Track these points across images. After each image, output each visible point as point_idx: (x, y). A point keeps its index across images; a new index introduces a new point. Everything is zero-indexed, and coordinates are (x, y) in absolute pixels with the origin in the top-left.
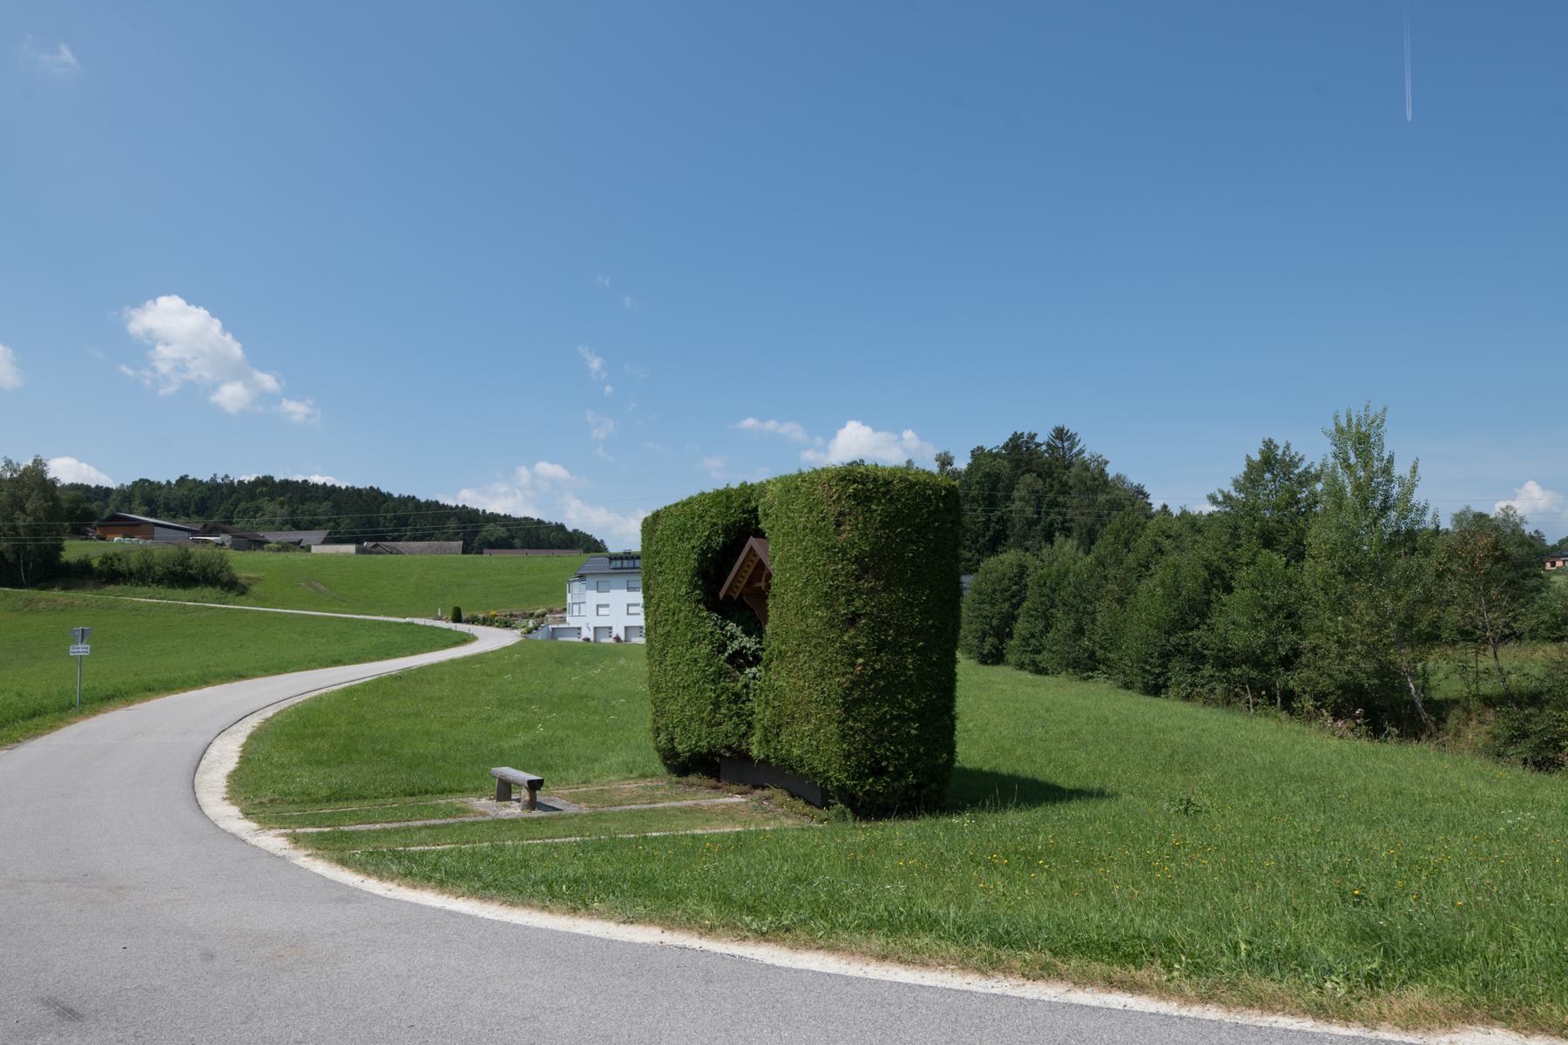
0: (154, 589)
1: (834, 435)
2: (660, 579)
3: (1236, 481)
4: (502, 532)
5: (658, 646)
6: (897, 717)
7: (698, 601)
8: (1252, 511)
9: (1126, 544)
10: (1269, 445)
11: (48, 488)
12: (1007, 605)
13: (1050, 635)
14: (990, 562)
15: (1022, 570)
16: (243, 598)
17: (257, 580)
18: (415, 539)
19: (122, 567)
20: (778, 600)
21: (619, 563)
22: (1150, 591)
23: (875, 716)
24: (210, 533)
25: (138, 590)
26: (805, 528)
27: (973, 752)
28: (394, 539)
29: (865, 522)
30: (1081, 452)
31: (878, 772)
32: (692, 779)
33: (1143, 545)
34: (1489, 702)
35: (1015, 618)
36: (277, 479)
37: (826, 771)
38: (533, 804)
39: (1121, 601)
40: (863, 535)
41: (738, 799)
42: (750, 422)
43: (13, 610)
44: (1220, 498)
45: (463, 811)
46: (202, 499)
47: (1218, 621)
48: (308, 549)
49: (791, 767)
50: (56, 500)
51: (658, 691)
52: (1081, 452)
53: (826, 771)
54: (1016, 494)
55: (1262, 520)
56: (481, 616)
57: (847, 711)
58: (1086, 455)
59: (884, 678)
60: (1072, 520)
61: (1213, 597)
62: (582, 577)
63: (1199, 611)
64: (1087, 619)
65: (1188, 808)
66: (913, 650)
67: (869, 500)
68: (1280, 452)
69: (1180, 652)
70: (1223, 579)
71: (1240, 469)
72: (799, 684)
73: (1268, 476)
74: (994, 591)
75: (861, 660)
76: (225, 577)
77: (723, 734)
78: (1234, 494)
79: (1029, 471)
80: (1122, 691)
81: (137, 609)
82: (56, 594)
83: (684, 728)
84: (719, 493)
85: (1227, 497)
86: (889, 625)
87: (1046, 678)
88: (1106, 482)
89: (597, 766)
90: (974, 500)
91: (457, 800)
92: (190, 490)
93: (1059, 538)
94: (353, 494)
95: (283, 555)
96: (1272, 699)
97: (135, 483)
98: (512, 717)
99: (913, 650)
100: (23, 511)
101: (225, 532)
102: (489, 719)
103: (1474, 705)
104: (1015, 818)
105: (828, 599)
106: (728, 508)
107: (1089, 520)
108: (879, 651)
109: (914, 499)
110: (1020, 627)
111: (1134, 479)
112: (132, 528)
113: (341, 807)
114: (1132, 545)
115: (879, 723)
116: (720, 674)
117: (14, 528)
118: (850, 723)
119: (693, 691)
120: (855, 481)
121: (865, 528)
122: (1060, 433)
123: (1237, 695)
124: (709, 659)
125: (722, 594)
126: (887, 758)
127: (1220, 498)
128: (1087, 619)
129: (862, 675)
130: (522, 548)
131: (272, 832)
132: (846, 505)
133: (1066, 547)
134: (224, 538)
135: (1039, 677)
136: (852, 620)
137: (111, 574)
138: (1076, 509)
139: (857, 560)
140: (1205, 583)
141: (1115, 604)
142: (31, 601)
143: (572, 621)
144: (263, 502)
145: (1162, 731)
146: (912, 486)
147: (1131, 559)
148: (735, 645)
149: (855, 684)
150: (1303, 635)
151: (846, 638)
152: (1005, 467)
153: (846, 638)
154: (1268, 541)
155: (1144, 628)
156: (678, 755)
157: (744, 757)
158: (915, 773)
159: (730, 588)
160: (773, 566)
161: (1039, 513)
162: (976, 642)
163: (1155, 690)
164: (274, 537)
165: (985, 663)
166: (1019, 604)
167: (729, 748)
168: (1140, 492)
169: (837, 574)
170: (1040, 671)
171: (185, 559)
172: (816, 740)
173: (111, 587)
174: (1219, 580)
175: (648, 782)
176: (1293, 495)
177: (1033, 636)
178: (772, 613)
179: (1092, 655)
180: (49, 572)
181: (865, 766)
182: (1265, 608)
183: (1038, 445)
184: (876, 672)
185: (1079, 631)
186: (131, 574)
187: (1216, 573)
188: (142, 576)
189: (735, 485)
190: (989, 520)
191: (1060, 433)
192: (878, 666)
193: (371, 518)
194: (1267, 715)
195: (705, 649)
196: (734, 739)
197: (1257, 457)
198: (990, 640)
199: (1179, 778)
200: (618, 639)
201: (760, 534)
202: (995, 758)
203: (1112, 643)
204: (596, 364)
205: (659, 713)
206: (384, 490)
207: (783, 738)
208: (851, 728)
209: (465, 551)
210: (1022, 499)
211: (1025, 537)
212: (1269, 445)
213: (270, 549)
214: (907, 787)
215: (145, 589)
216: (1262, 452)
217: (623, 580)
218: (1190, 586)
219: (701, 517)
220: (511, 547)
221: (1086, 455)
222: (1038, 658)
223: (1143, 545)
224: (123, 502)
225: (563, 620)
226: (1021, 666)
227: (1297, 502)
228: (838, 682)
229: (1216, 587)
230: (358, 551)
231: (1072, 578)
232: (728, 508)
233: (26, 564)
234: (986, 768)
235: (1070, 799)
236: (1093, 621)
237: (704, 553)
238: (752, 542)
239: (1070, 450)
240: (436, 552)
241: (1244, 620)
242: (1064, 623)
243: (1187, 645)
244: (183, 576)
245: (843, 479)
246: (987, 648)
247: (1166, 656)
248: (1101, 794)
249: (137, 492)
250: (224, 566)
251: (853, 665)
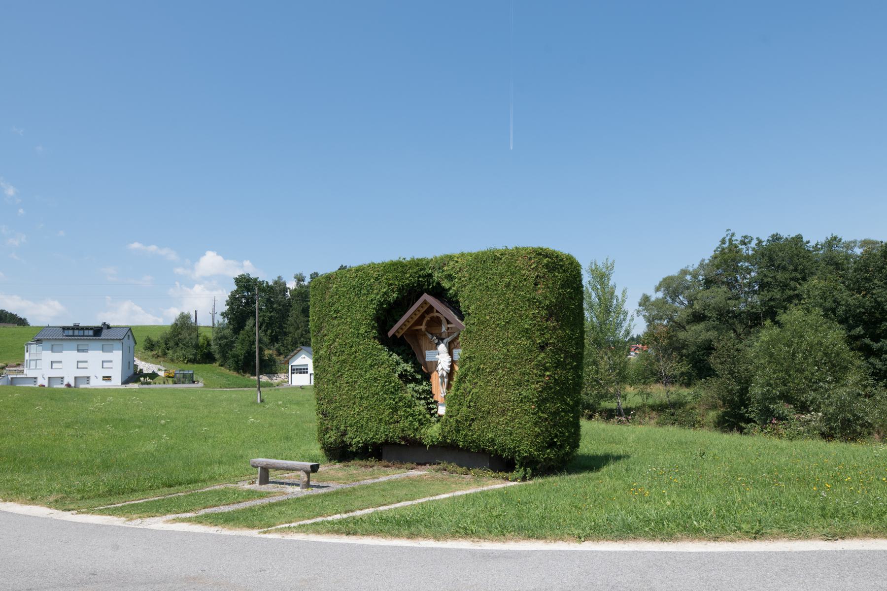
1: (198, 260)
7: (374, 338)
21: (71, 332)
31: (551, 445)
34: (653, 408)
42: (136, 245)
57: (539, 407)
62: (39, 341)
75: (548, 373)
103: (647, 410)
108: (557, 367)
115: (556, 413)
125: (390, 334)
131: (165, 518)
136: (542, 348)
139: (548, 308)
143: (28, 373)
149: (544, 389)
167: (404, 438)
169: (535, 317)
200: (69, 385)
204: (11, 191)
217: (74, 344)
225: (22, 372)
237: (381, 304)
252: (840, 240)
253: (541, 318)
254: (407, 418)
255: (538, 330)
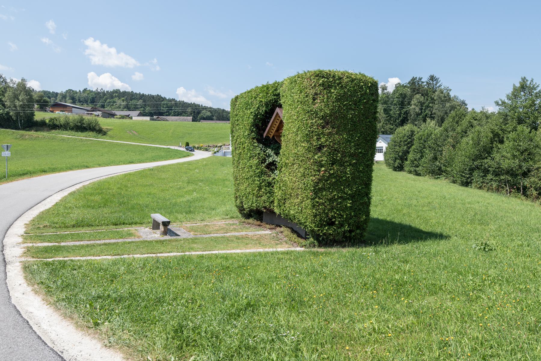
0: (70, 132)
2: (237, 128)
3: (508, 96)
4: (209, 114)
5: (236, 159)
6: (341, 197)
7: (254, 138)
8: (514, 108)
9: (457, 123)
10: (524, 80)
11: (29, 92)
12: (405, 147)
13: (423, 160)
14: (400, 129)
15: (413, 132)
16: (104, 136)
17: (111, 129)
18: (175, 116)
19: (57, 123)
20: (286, 138)
22: (467, 141)
23: (330, 197)
24: (93, 111)
25: (64, 132)
26: (298, 101)
27: (384, 210)
28: (167, 116)
29: (328, 98)
30: (440, 86)
31: (331, 223)
32: (251, 220)
33: (465, 123)
35: (408, 153)
36: (121, 91)
37: (305, 222)
38: (165, 233)
39: (454, 146)
40: (327, 105)
41: (268, 232)
43: (16, 139)
44: (500, 103)
45: (130, 235)
46: (93, 98)
47: (497, 156)
48: (131, 118)
49: (290, 219)
50: (31, 96)
51: (236, 180)
52: (440, 86)
53: (305, 222)
54: (412, 102)
55: (519, 112)
56: (197, 146)
57: (316, 193)
58: (442, 87)
59: (335, 177)
60: (435, 114)
61: (494, 145)
63: (488, 151)
64: (438, 153)
65: (486, 248)
66: (350, 165)
67: (330, 87)
68: (528, 83)
69: (478, 168)
70: (499, 137)
71: (510, 90)
72: (295, 179)
73: (522, 93)
74: (401, 141)
75: (323, 169)
76: (97, 128)
77: (262, 202)
78: (506, 101)
79: (418, 93)
80: (452, 184)
81: (63, 140)
82: (32, 133)
83: (246, 198)
84: (264, 86)
85: (504, 103)
86: (338, 152)
87: (420, 177)
88: (450, 98)
89: (214, 212)
90: (395, 104)
91: (132, 229)
92: (88, 94)
93: (428, 120)
94: (151, 97)
95: (121, 120)
96: (518, 189)
97: (67, 91)
98: (190, 188)
99: (350, 165)
100: (18, 100)
101: (99, 111)
102: (180, 188)
104: (397, 249)
105: (308, 137)
106: (267, 93)
107: (442, 114)
108: (333, 164)
109: (354, 87)
110: (411, 156)
111: (461, 98)
112: (63, 107)
113: (82, 231)
114: (460, 123)
115: (331, 200)
116: (262, 173)
117: (15, 106)
118: (317, 200)
119: (250, 180)
120: (323, 77)
121: (328, 101)
122: (432, 78)
123: (503, 188)
124: (257, 165)
126: (335, 217)
127: (500, 103)
128: (438, 153)
129: (323, 176)
130: (217, 120)
132: (319, 89)
133: (431, 124)
134: (99, 113)
135: (417, 177)
136: (320, 148)
137: (54, 126)
138: (436, 109)
139: (323, 118)
140: (491, 139)
141: (451, 148)
142: (23, 135)
144: (116, 99)
145: (469, 203)
146: (353, 80)
147: (459, 129)
148: (271, 160)
150: (535, 162)
151: (316, 157)
152: (408, 91)
153: (316, 157)
154: (520, 121)
155: (463, 158)
156: (244, 210)
157: (272, 212)
158: (349, 225)
159: (268, 132)
160: (284, 121)
161: (421, 109)
162: (392, 162)
163: (466, 184)
164: (119, 113)
165: (396, 170)
166: (411, 147)
167: (265, 208)
168: (464, 103)
170: (418, 174)
171: (82, 120)
172: (300, 206)
173: (54, 131)
174: (498, 138)
175: (231, 222)
176: (533, 101)
177: (416, 160)
178: (283, 144)
179: (440, 169)
180: (30, 124)
181: (324, 221)
182: (518, 150)
183: (423, 82)
184: (331, 175)
185: (435, 158)
186: (61, 126)
187: (496, 135)
188: (65, 127)
189: (271, 82)
190: (401, 113)
191: (432, 78)
192: (332, 172)
193: (158, 108)
194: (516, 197)
195: (255, 161)
196: (268, 204)
197: (518, 85)
198: (398, 161)
199: (479, 227)
201: (280, 106)
202: (393, 214)
203: (449, 163)
205: (237, 190)
206: (163, 96)
207: (287, 205)
208: (317, 202)
209: (193, 121)
210: (415, 105)
211: (415, 120)
212: (524, 80)
213: (117, 118)
214: (345, 232)
215: (67, 132)
216: (520, 83)
218: (484, 141)
219: (255, 98)
220: (212, 119)
221: (442, 87)
222: (417, 169)
223: (465, 123)
224: (62, 98)
226: (410, 172)
227: (535, 105)
228: (311, 180)
229: (496, 141)
230: (151, 120)
231: (433, 136)
232: (267, 93)
233: (21, 121)
234: (388, 219)
235: (426, 239)
236: (441, 154)
237: (256, 115)
238: (278, 110)
239: (436, 85)
240: (182, 120)
241: (509, 155)
242: (429, 155)
243: (482, 165)
244: (81, 127)
245: (317, 76)
246: (396, 164)
247: (472, 170)
248: (440, 236)
249: (68, 95)
250: (97, 124)
251: (319, 171)
252: (80, 91)
253: (317, 126)
254: (266, 194)
255: (316, 135)
